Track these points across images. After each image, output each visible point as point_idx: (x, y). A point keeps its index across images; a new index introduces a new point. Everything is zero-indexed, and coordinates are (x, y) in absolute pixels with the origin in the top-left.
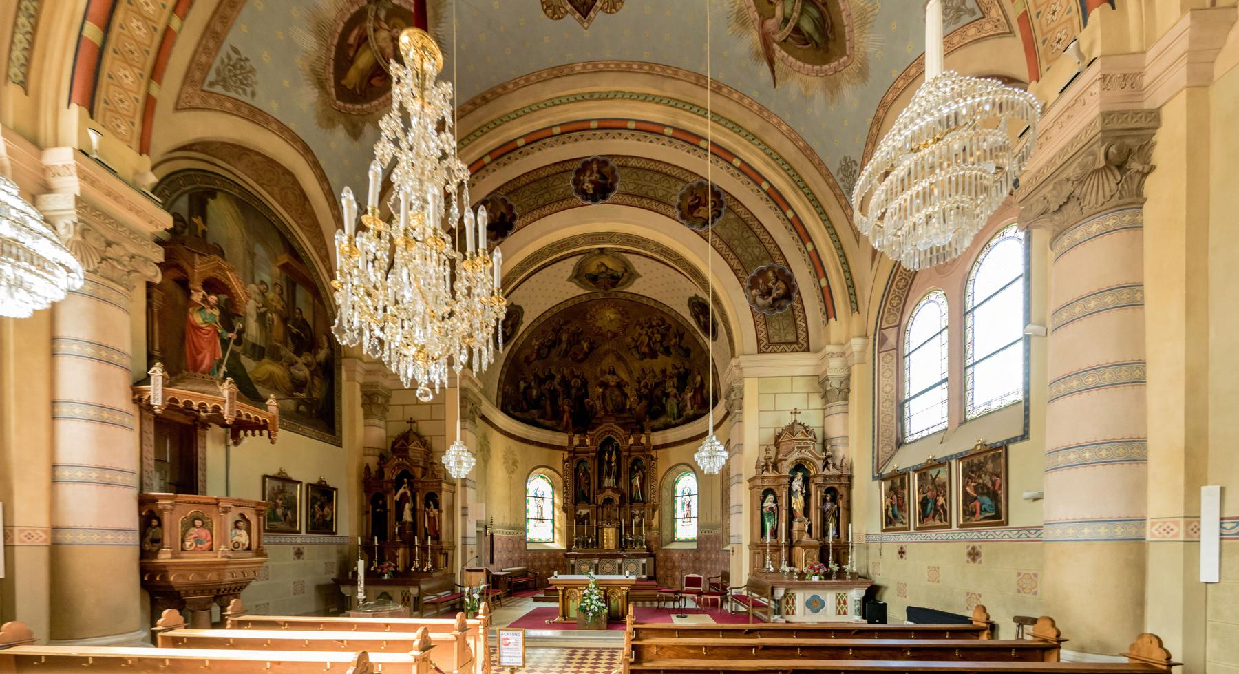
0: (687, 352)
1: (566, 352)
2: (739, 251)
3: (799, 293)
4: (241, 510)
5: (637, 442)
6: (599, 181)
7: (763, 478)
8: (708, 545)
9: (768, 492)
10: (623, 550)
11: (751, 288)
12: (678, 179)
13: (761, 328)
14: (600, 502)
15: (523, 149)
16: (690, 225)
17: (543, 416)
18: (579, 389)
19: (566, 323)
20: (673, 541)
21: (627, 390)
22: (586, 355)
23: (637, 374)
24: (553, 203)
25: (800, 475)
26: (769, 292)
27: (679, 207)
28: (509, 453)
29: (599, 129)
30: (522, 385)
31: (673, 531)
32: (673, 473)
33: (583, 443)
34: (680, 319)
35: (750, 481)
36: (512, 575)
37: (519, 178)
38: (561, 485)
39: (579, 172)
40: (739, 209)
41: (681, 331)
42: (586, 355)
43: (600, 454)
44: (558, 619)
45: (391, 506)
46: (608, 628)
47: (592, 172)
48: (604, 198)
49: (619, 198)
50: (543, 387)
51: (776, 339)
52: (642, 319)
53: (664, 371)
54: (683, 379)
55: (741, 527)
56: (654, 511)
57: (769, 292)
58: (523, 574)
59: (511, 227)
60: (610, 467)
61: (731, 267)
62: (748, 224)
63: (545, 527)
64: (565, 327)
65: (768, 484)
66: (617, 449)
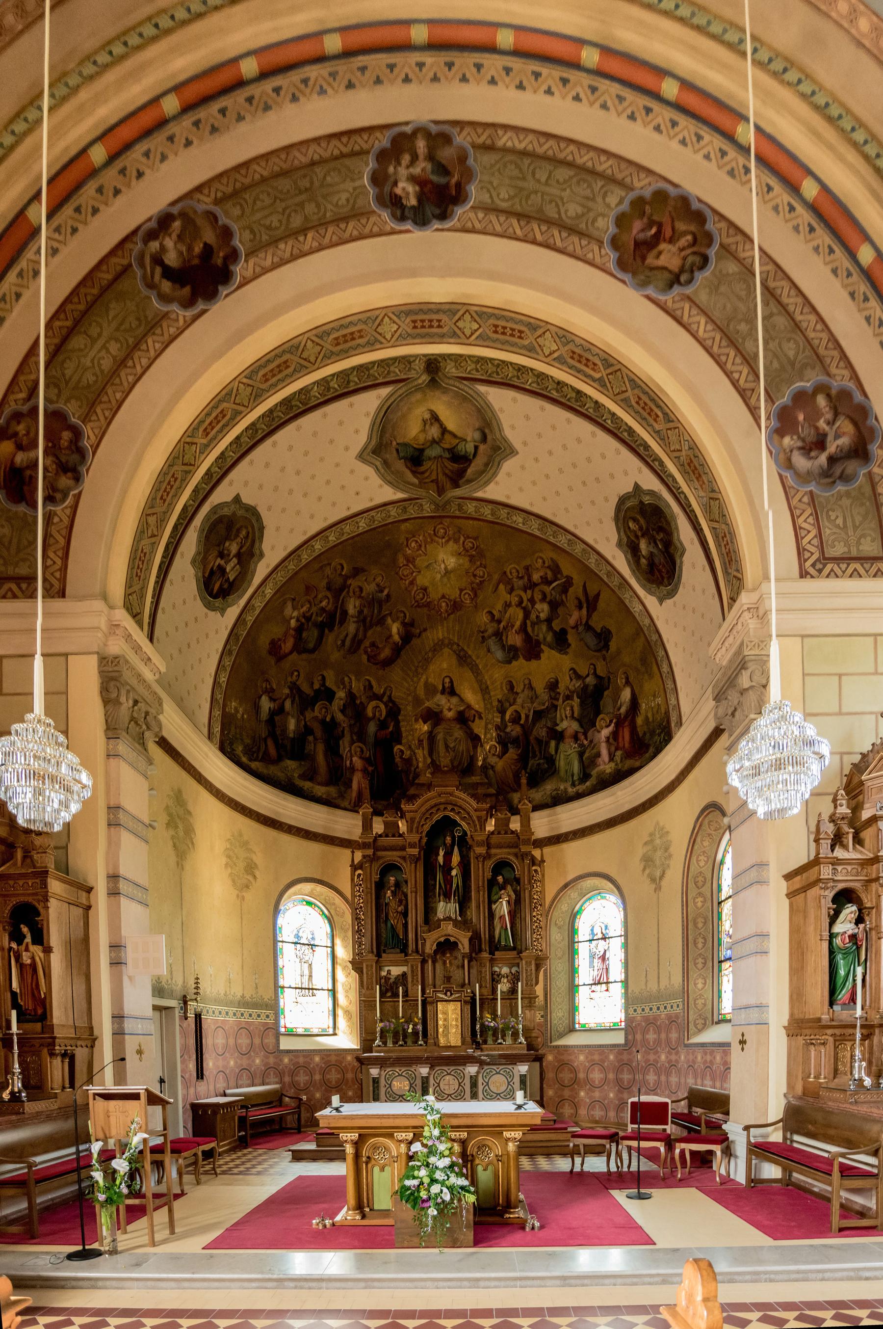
0: (604, 638)
1: (356, 645)
5: (503, 827)
6: (433, 181)
7: (836, 862)
8: (651, 1036)
9: (844, 897)
10: (478, 1046)
12: (612, 180)
13: (806, 522)
14: (430, 948)
15: (255, 90)
16: (642, 285)
17: (310, 775)
18: (382, 725)
19: (357, 572)
20: (572, 1030)
21: (478, 727)
22: (397, 651)
23: (498, 693)
24: (324, 224)
26: (820, 444)
27: (615, 243)
28: (239, 841)
29: (433, 46)
30: (266, 704)
31: (573, 1009)
32: (572, 894)
33: (391, 829)
34: (592, 562)
35: (788, 877)
36: (247, 1103)
37: (246, 164)
38: (348, 918)
39: (383, 156)
41: (592, 589)
42: (397, 651)
43: (429, 851)
44: (345, 1215)
46: (477, 1243)
47: (415, 158)
48: (443, 216)
50: (309, 715)
51: (838, 550)
52: (510, 568)
53: (553, 686)
54: (592, 699)
56: (538, 967)
57: (820, 444)
58: (274, 1100)
59: (223, 276)
60: (448, 879)
61: (735, 384)
63: (317, 999)
64: (354, 583)
65: (845, 878)
66: (463, 843)
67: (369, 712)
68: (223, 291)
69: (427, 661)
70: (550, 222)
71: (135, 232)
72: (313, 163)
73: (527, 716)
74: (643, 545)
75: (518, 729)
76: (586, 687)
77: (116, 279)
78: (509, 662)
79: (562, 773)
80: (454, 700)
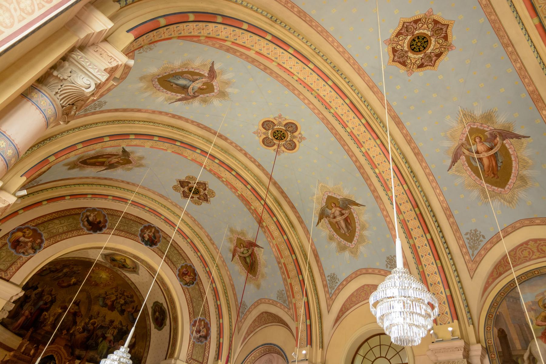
1: (58, 278)
2: (194, 305)
3: (210, 338)
6: (152, 238)
12: (183, 258)
16: (181, 281)
18: (46, 304)
21: (78, 320)
22: (69, 285)
27: (179, 270)
39: (145, 227)
40: (201, 286)
47: (151, 232)
48: (151, 246)
49: (157, 250)
51: (194, 357)
53: (112, 322)
59: (100, 229)
61: (189, 311)
62: (202, 294)
67: (44, 298)
68: (98, 232)
70: (170, 259)
71: (86, 208)
72: (131, 220)
73: (98, 325)
74: (157, 314)
75: (92, 327)
76: (122, 329)
77: (76, 214)
78: (103, 307)
79: (99, 351)
80: (77, 307)
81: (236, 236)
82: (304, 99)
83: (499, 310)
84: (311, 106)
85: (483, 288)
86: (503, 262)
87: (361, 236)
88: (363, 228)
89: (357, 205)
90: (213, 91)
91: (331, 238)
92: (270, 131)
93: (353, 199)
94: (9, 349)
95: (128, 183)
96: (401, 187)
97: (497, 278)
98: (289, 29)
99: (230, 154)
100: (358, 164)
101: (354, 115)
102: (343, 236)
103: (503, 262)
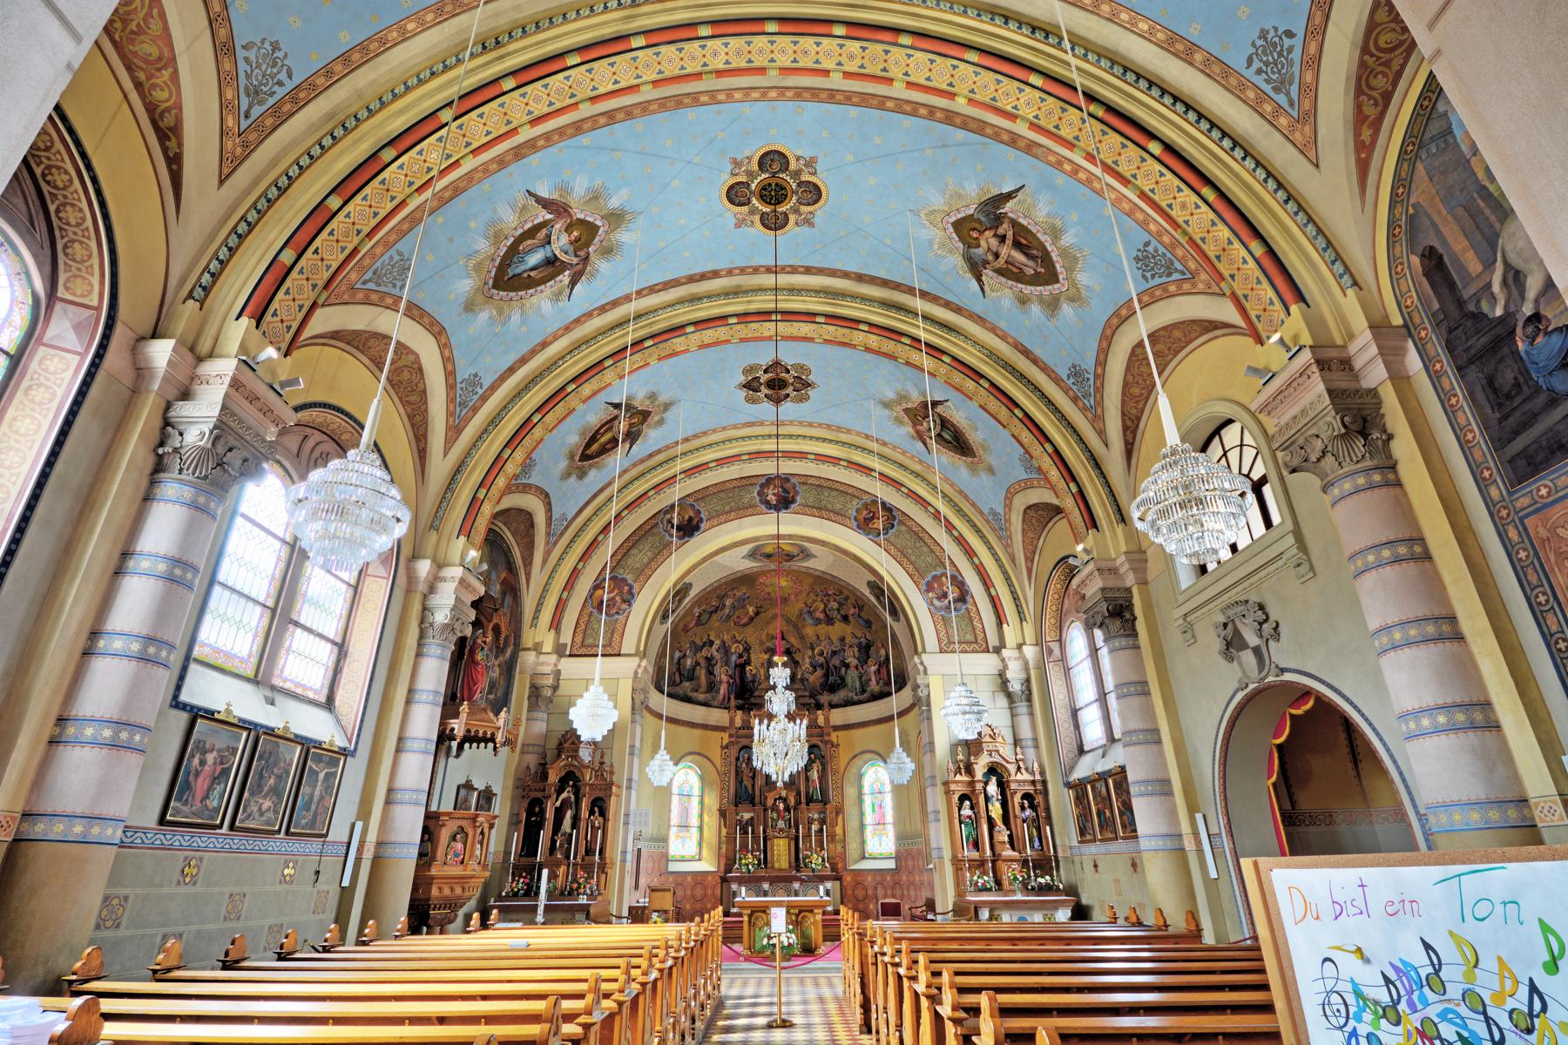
0: (869, 624)
1: (729, 617)
4: (460, 823)
8: (910, 863)
11: (928, 591)
18: (741, 656)
25: (994, 779)
31: (863, 842)
32: (858, 762)
39: (762, 486)
40: (910, 523)
45: (550, 814)
53: (843, 639)
55: (940, 837)
56: (837, 814)
59: (697, 528)
69: (768, 623)
81: (899, 408)
82: (729, 96)
83: (1413, 200)
84: (755, 95)
85: (1354, 169)
86: (1370, 61)
87: (1064, 253)
88: (1056, 233)
89: (1009, 196)
90: (598, 228)
91: (1023, 301)
92: (754, 201)
93: (995, 192)
94: (723, 729)
95: (705, 433)
96: (1028, 89)
97: (1382, 114)
98: (537, 27)
99: (746, 292)
100: (939, 115)
101: (811, 40)
102: (1036, 280)
103: (1370, 61)
